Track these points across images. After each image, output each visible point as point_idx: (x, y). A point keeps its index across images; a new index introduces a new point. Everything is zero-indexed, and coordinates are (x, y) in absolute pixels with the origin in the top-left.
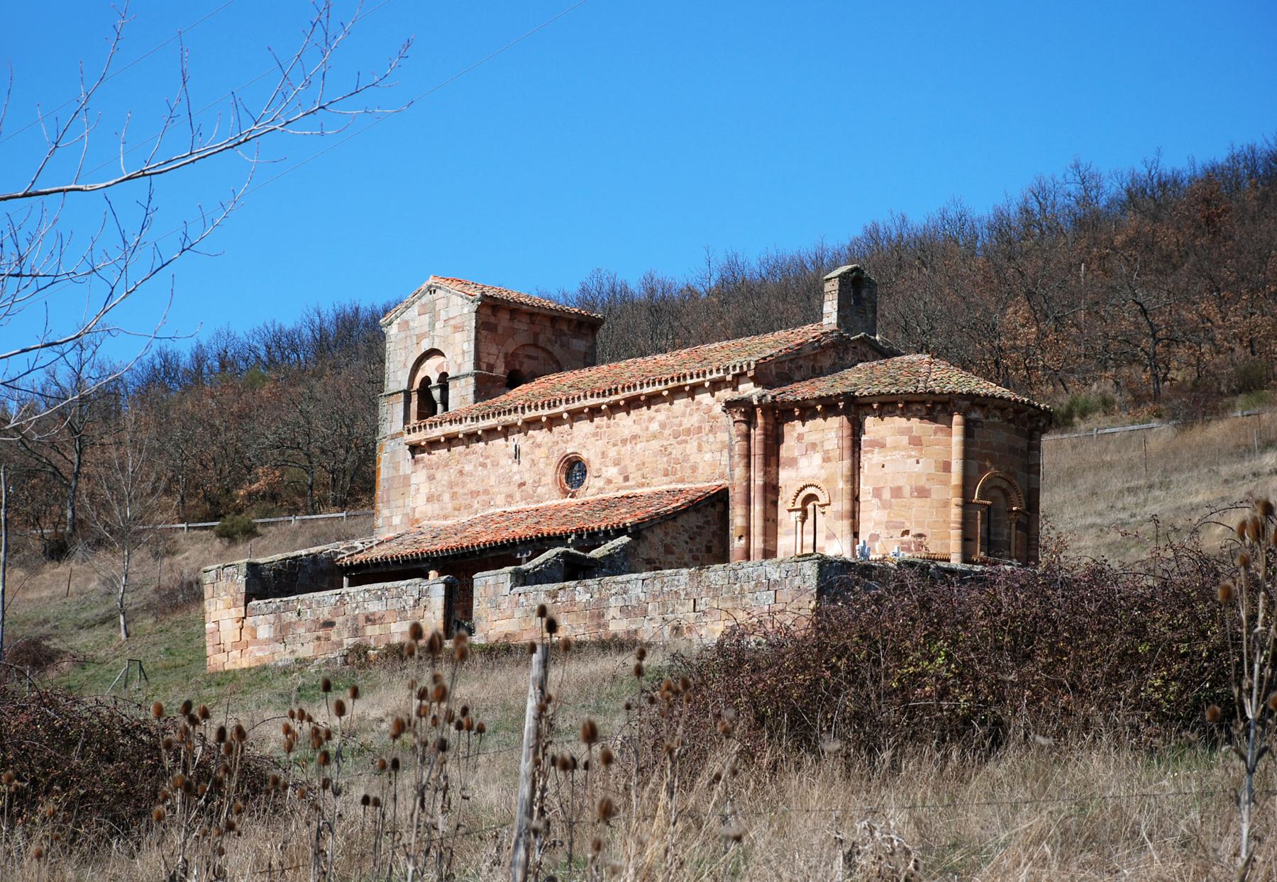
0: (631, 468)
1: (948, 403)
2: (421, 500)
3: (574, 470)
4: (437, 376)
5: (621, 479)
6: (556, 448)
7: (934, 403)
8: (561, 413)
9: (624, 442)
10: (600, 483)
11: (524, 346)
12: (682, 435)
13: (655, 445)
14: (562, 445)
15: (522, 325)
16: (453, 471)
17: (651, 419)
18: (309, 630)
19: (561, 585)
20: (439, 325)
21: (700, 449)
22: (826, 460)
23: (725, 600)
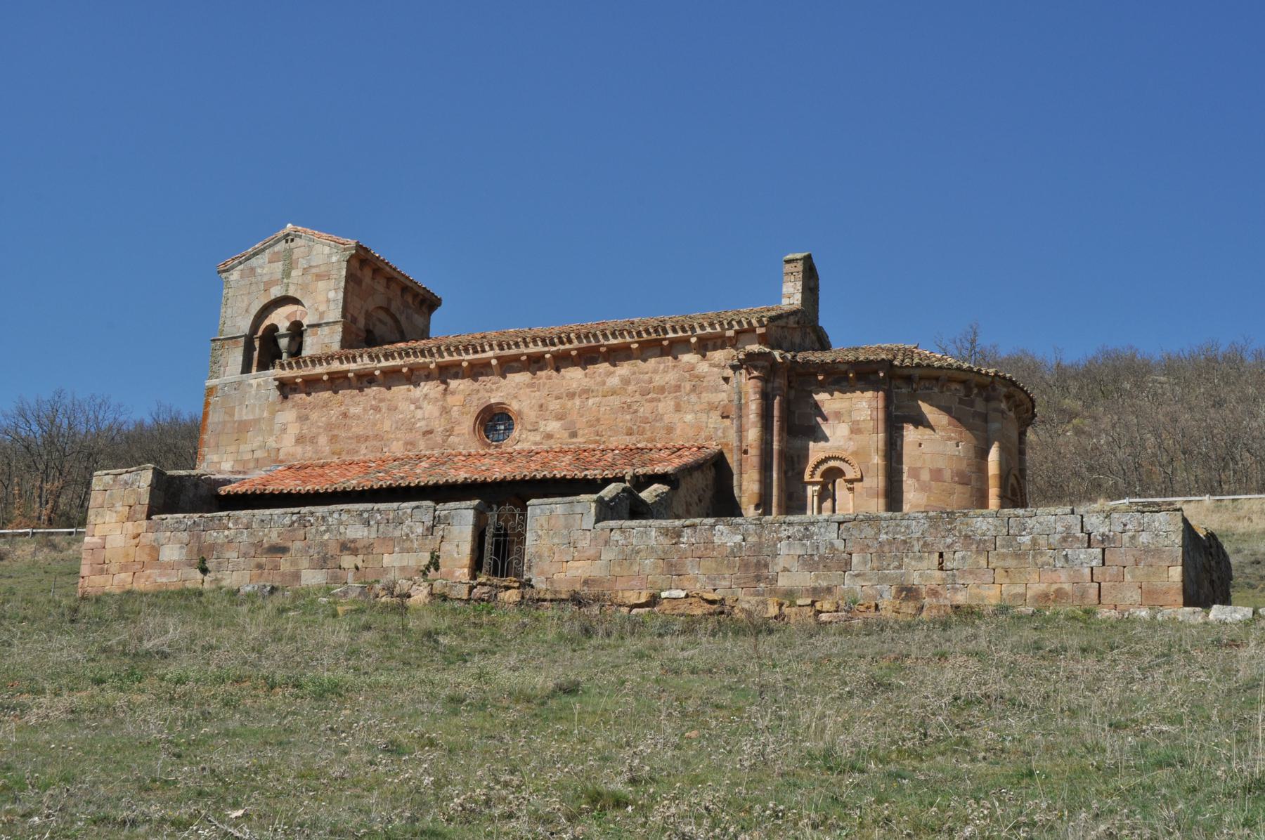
0: (581, 423)
3: (494, 421)
4: (287, 324)
5: (566, 435)
6: (475, 397)
9: (572, 395)
13: (615, 401)
14: (482, 393)
15: (380, 286)
16: (334, 412)
17: (611, 374)
18: (245, 555)
21: (678, 408)
22: (855, 430)
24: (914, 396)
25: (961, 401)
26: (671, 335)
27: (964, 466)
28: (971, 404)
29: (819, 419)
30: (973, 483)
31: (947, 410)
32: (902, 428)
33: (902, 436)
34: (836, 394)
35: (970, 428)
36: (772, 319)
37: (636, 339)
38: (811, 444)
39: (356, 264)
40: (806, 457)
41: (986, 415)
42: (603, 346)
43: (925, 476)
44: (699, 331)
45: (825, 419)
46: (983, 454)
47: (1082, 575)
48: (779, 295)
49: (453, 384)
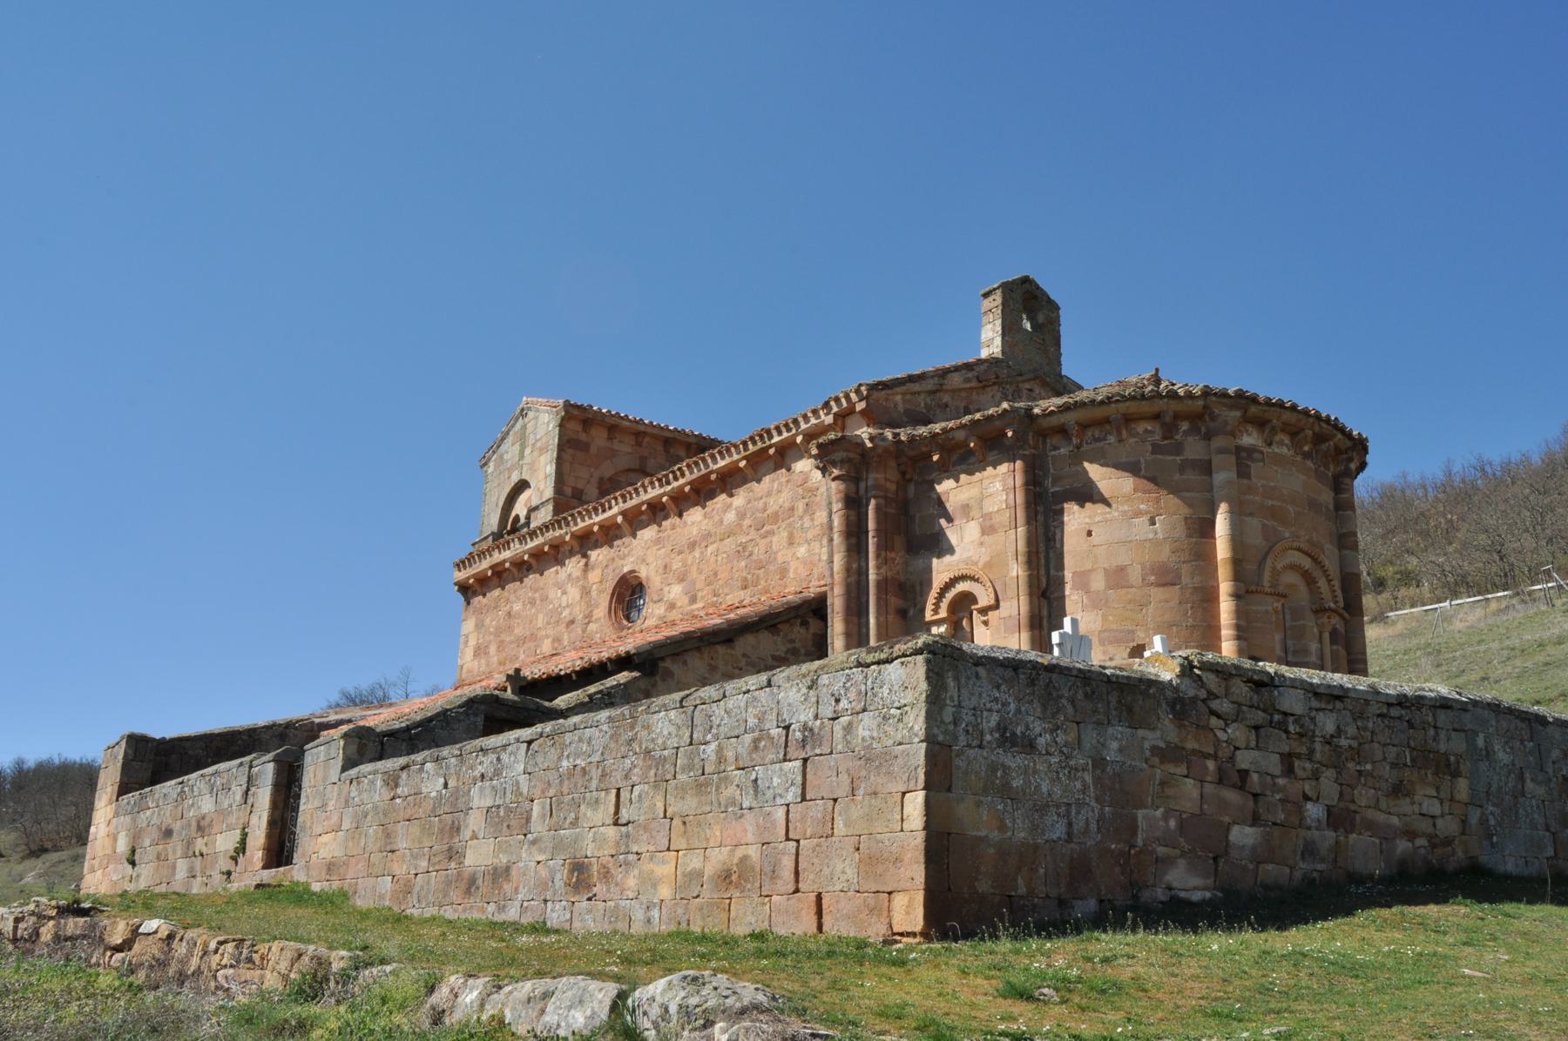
1: (1200, 417)
2: (469, 653)
7: (1177, 417)
8: (615, 516)
9: (692, 546)
10: (660, 610)
11: (629, 470)
12: (766, 523)
19: (402, 761)
20: (527, 451)
21: (791, 542)
22: (987, 530)
23: (682, 791)
24: (1078, 457)
25: (1156, 449)
26: (776, 439)
27: (1165, 554)
28: (1178, 449)
29: (943, 522)
30: (1185, 580)
31: (1132, 468)
32: (1061, 512)
33: (1062, 523)
34: (963, 477)
35: (1174, 490)
36: (873, 387)
37: (743, 454)
38: (935, 561)
39: (574, 426)
40: (927, 583)
41: (1210, 462)
42: (711, 472)
43: (1098, 583)
44: (803, 426)
45: (950, 520)
46: (1205, 528)
47: (774, 823)
48: (978, 345)
49: (594, 555)
